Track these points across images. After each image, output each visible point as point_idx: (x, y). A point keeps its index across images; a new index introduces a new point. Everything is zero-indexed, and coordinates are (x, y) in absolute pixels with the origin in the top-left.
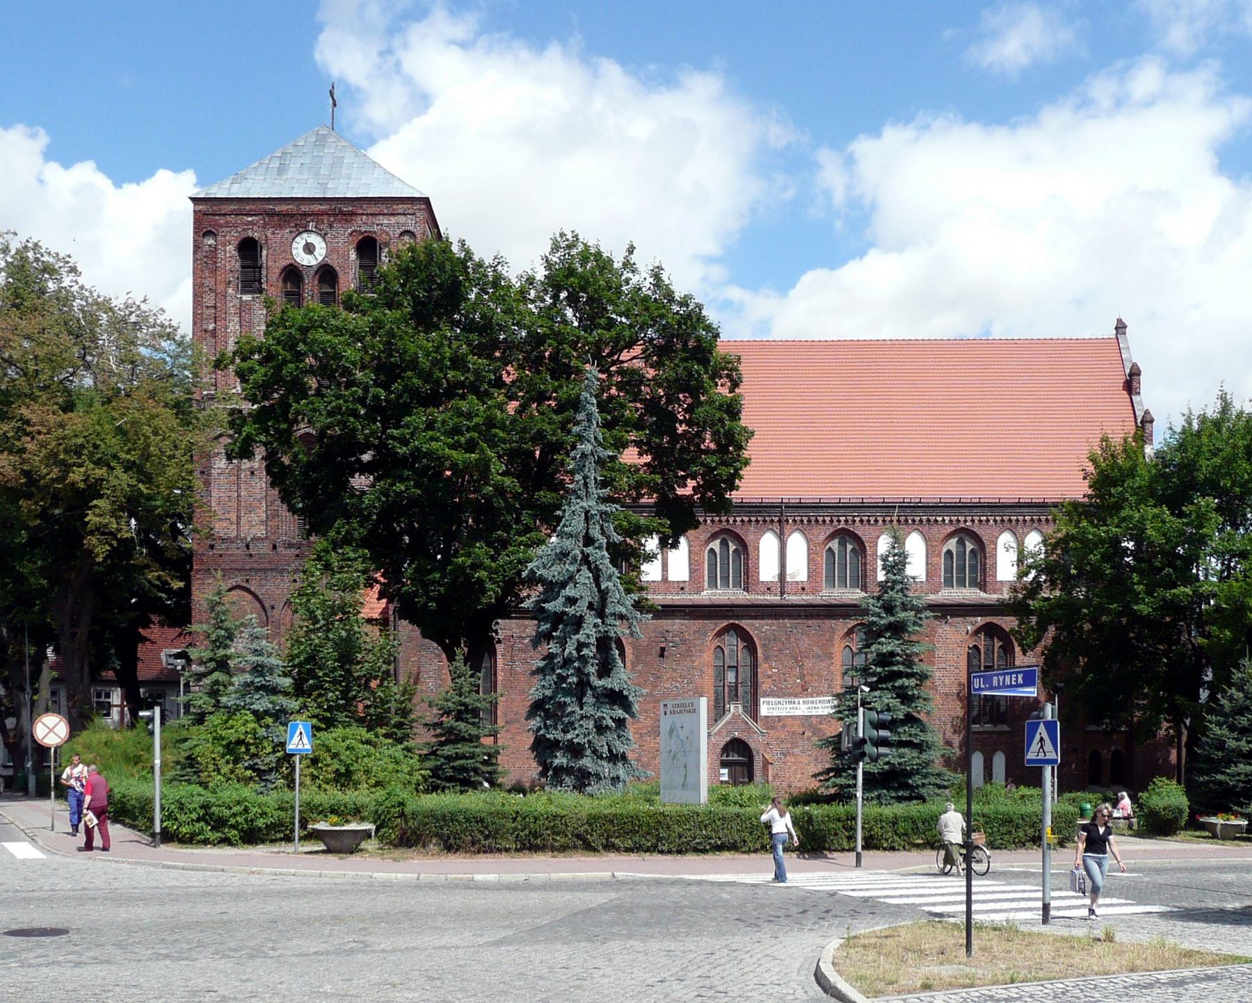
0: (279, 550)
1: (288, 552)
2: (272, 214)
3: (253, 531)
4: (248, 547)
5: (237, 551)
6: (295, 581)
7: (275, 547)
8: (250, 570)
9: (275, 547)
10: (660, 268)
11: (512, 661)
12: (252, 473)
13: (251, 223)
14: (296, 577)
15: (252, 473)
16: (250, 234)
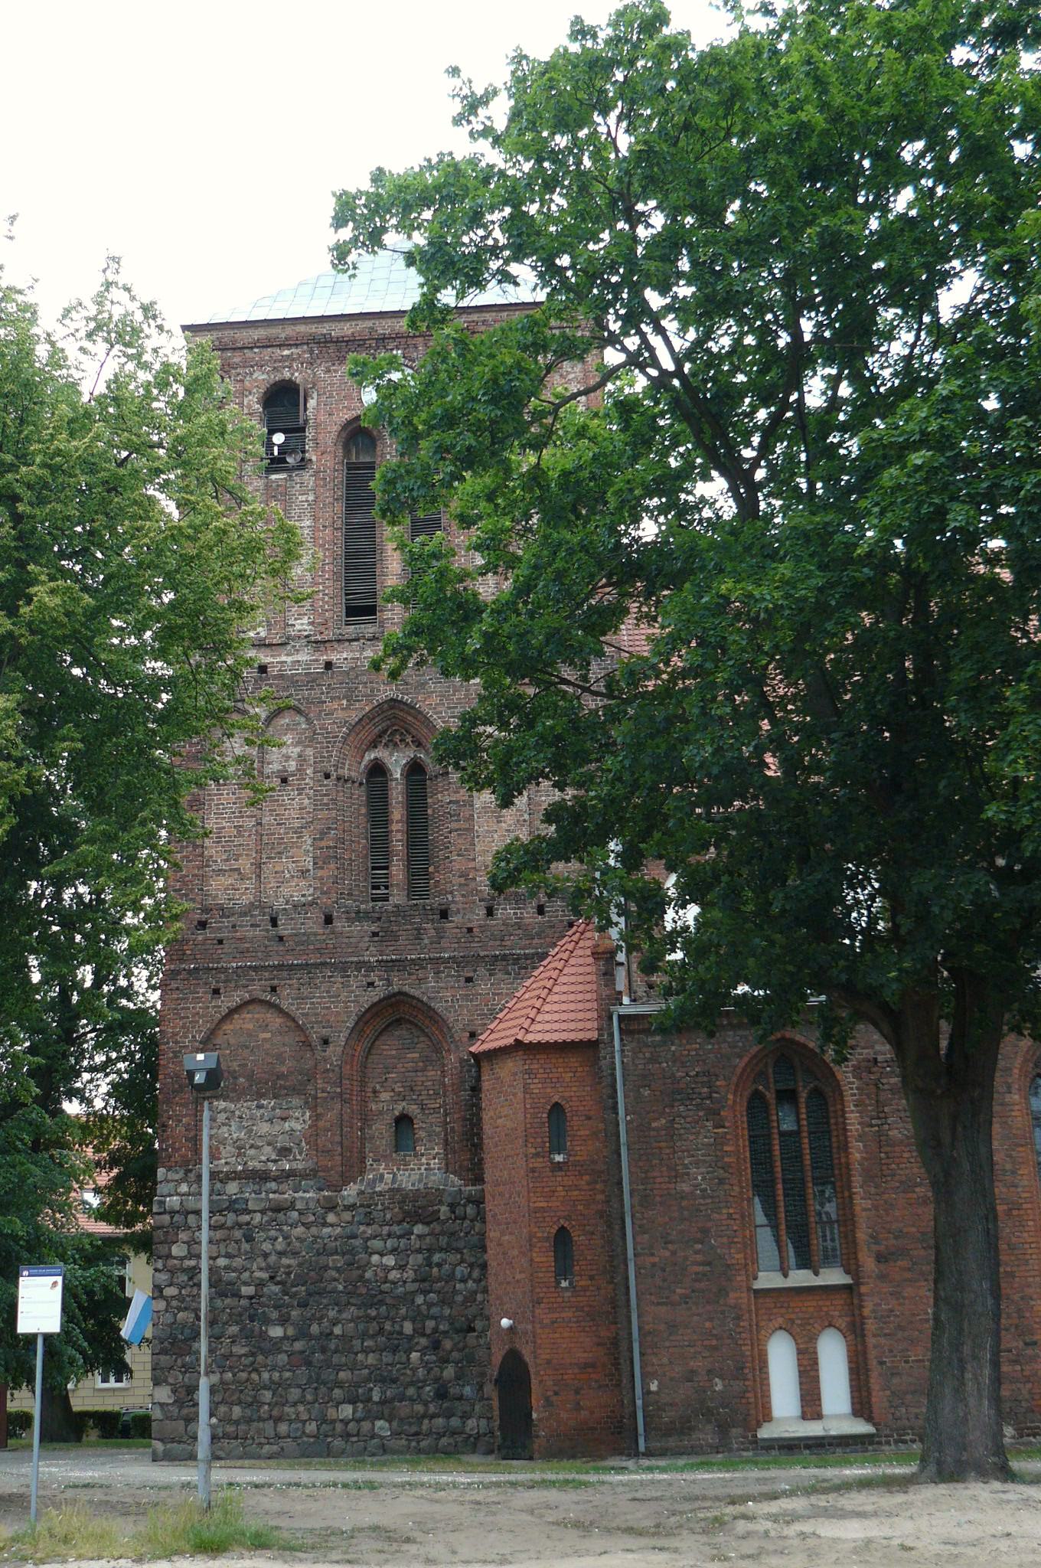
0: (339, 925)
1: (357, 927)
2: (325, 341)
3: (285, 891)
4: (274, 922)
5: (253, 932)
6: (371, 984)
7: (329, 920)
8: (280, 967)
9: (329, 920)
10: (578, 20)
11: (881, 1115)
12: (284, 781)
13: (284, 358)
14: (373, 977)
15: (284, 781)
16: (287, 374)
